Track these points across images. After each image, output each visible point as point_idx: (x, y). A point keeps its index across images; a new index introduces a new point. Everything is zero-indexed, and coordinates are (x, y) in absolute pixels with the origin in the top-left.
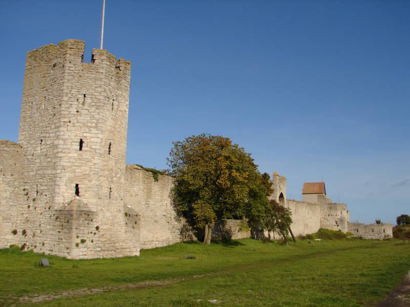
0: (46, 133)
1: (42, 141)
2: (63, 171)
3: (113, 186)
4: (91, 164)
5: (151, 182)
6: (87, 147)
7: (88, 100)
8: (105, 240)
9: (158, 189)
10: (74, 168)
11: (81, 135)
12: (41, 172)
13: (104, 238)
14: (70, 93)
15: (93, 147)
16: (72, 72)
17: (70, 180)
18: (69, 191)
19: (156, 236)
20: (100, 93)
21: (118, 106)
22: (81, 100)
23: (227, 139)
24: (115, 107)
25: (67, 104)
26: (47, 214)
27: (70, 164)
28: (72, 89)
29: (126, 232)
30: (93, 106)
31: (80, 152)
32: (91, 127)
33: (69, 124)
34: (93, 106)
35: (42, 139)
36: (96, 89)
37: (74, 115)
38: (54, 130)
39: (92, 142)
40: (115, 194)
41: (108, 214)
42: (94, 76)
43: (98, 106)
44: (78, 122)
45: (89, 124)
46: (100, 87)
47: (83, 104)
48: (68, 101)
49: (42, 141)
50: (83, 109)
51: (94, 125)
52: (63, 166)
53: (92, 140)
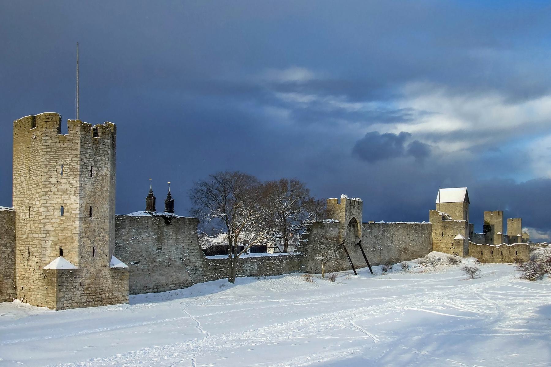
0: (33, 200)
1: (30, 207)
2: (48, 235)
3: (95, 244)
4: (72, 228)
5: (162, 227)
6: (68, 212)
7: (67, 170)
8: (89, 292)
9: (171, 233)
10: (57, 232)
11: (62, 202)
12: (31, 235)
13: (89, 291)
14: (49, 164)
15: (73, 212)
16: (49, 144)
17: (55, 243)
18: (54, 252)
19: (171, 279)
20: (77, 163)
21: (98, 171)
22: (60, 171)
23: (191, 199)
24: (94, 172)
25: (47, 175)
26: (38, 273)
27: (53, 229)
28: (51, 160)
29: (113, 283)
30: (71, 175)
31: (63, 218)
32: (71, 194)
33: (50, 193)
34: (71, 175)
35: (31, 205)
36: (73, 159)
37: (55, 184)
38: (39, 199)
39: (72, 208)
40: (98, 251)
41: (92, 270)
42: (70, 146)
43: (76, 175)
44: (58, 191)
45: (68, 192)
46: (77, 157)
47: (62, 174)
48: (48, 172)
49: (30, 207)
50: (62, 179)
51: (73, 192)
52: (48, 231)
53: (72, 206)
